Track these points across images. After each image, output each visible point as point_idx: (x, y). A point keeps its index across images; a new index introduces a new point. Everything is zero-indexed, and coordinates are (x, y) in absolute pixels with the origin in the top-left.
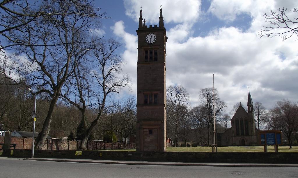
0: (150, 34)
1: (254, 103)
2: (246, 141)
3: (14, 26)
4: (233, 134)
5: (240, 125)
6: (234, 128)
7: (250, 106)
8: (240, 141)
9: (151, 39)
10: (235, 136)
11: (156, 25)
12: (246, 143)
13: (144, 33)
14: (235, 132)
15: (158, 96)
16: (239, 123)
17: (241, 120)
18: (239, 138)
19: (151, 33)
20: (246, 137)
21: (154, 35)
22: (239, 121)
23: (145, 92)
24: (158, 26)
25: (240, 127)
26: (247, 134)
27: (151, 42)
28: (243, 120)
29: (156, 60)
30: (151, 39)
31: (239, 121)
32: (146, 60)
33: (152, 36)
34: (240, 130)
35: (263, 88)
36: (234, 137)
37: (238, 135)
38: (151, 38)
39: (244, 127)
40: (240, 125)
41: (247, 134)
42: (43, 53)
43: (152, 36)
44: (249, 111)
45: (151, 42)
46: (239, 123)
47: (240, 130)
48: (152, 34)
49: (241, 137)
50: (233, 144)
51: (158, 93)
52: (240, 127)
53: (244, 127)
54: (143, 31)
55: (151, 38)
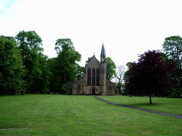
5: (92, 75)
7: (102, 57)
8: (90, 90)
12: (96, 93)
25: (91, 76)
28: (95, 70)
40: (92, 75)
52: (91, 76)
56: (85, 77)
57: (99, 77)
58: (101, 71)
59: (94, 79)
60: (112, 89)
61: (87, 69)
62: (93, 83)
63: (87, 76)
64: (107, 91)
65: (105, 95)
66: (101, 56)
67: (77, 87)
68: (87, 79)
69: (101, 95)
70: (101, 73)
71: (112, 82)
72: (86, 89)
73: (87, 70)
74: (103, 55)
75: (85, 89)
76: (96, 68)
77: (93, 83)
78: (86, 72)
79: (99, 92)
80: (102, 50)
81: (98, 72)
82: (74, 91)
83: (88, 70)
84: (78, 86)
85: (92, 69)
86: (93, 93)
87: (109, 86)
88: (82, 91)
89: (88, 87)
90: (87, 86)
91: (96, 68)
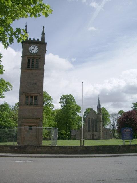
0: (33, 46)
5: (91, 124)
8: (90, 136)
9: (34, 49)
11: (39, 39)
12: (95, 137)
13: (28, 44)
15: (37, 97)
16: (91, 122)
17: (92, 120)
18: (90, 133)
19: (34, 45)
20: (95, 133)
21: (37, 47)
22: (94, 121)
23: (26, 94)
24: (40, 40)
26: (96, 131)
27: (31, 51)
28: (90, 120)
29: (37, 67)
30: (34, 49)
31: (94, 121)
32: (29, 67)
33: (35, 48)
34: (91, 128)
35: (95, 7)
36: (86, 133)
37: (89, 131)
38: (34, 49)
39: (94, 125)
40: (91, 124)
41: (96, 131)
43: (35, 48)
45: (31, 51)
46: (91, 122)
47: (91, 128)
48: (35, 46)
49: (91, 133)
51: (38, 95)
53: (94, 125)
54: (27, 44)
55: (34, 49)
57: (97, 125)
59: (93, 127)
62: (93, 130)
68: (87, 127)
76: (94, 118)
85: (91, 119)
91: (94, 118)
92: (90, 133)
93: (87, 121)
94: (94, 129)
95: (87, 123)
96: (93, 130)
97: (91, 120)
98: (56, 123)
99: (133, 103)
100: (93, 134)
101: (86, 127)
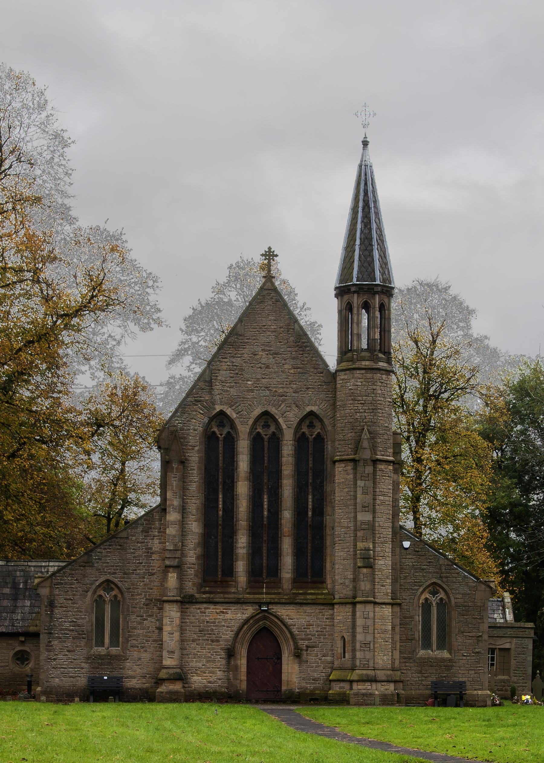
1: (406, 263)
2: (298, 655)
3: (396, 672)
4: (172, 578)
5: (243, 489)
6: (183, 510)
7: (356, 301)
8: (230, 654)
10: (186, 601)
12: (292, 674)
14: (192, 556)
16: (243, 464)
22: (288, 450)
25: (243, 506)
28: (276, 440)
31: (288, 450)
34: (242, 541)
36: (172, 613)
39: (287, 515)
40: (243, 489)
42: (349, 608)
44: (345, 351)
46: (243, 464)
47: (242, 541)
50: (159, 682)
52: (243, 506)
53: (287, 515)
56: (173, 516)
57: (319, 511)
58: (338, 446)
59: (264, 532)
60: (457, 640)
61: (195, 427)
62: (264, 570)
63: (195, 504)
64: (408, 656)
65: (387, 701)
66: (342, 292)
67: (87, 620)
68: (195, 527)
69: (342, 700)
70: (341, 474)
71: (279, 672)
72: (190, 634)
73: (208, 443)
74: (364, 288)
75: (171, 640)
76: (288, 421)
77: (255, 573)
78: (183, 462)
79: (319, 673)
80: (359, 176)
81: (350, 254)
82: (65, 664)
83: (210, 438)
84: (99, 602)
85: (243, 430)
86: (260, 683)
87: (427, 606)
88: (146, 656)
89: (211, 613)
90: (193, 608)
91: (288, 421)
92: (231, 619)
93: (195, 457)
94: (274, 571)
95: (195, 484)
96: (264, 570)
97: (243, 446)
98: (61, 352)
99: (270, 248)
100: (349, 302)
101: (182, 524)
